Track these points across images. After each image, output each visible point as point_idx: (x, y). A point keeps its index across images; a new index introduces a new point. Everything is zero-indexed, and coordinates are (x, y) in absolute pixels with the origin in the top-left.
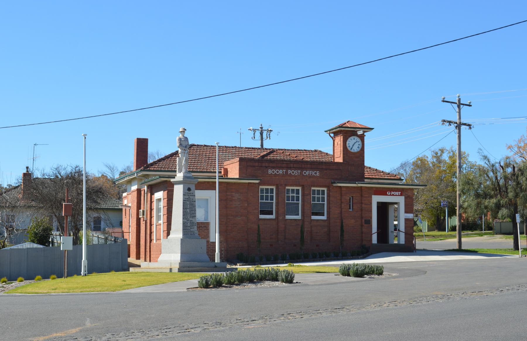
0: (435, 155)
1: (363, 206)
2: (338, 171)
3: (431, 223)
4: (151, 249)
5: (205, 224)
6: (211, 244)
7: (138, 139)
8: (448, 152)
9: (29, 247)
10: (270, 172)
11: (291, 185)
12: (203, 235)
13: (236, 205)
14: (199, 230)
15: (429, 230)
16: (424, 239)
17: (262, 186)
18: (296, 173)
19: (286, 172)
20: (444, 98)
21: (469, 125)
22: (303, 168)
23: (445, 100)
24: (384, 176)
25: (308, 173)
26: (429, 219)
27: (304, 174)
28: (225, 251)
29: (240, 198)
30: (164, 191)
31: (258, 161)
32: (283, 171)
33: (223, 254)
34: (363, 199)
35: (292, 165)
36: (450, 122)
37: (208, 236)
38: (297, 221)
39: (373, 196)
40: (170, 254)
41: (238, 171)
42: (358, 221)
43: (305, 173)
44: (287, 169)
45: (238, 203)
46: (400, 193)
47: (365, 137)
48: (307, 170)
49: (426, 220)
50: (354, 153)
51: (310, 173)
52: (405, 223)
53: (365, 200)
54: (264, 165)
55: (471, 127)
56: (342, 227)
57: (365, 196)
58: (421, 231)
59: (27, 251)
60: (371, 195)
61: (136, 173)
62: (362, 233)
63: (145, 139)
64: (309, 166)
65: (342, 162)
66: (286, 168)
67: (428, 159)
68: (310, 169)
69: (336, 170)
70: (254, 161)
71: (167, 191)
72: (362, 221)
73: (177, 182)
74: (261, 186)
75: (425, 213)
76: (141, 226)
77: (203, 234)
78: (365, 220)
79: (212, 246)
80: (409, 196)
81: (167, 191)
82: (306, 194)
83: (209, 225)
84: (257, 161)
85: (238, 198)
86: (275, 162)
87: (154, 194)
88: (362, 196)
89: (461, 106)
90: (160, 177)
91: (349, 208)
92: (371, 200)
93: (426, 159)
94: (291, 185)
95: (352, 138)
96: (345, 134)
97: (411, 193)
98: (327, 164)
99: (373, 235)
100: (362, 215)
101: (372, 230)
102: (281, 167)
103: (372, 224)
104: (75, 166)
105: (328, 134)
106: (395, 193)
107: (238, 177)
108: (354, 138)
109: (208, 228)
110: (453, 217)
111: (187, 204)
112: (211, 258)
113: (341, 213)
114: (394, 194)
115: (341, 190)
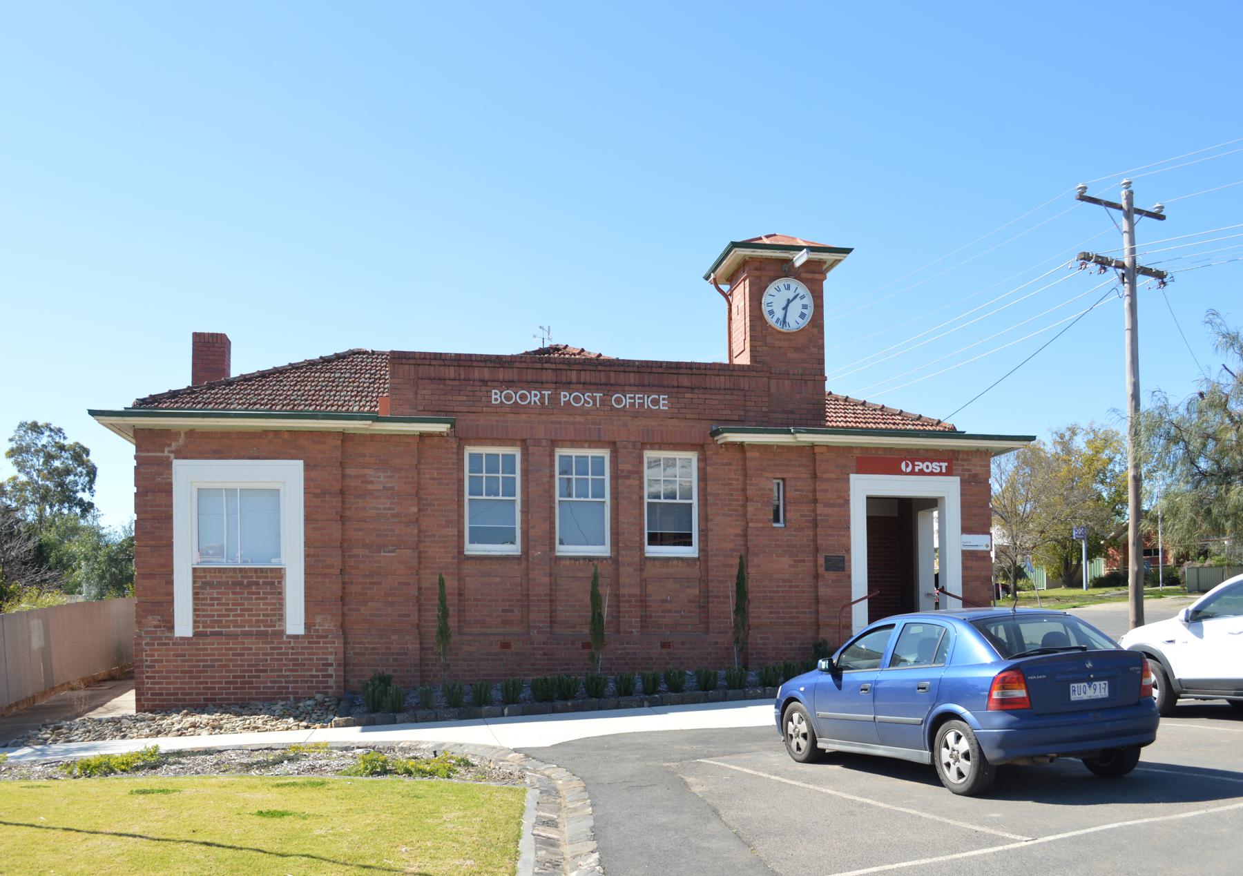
0: (1060, 440)
1: (820, 509)
2: (732, 394)
3: (1054, 573)
6: (290, 642)
8: (1085, 432)
10: (496, 400)
11: (572, 441)
12: (262, 613)
13: (379, 509)
15: (1050, 586)
16: (1039, 605)
17: (474, 445)
18: (589, 403)
19: (554, 399)
20: (1085, 188)
21: (1160, 275)
22: (612, 385)
23: (1088, 194)
24: (904, 424)
25: (628, 401)
26: (1049, 563)
27: (577, 394)
28: (339, 665)
29: (392, 488)
32: (542, 397)
33: (331, 676)
34: (817, 488)
35: (573, 376)
36: (1103, 263)
38: (596, 562)
39: (853, 477)
42: (804, 561)
43: (619, 401)
44: (556, 389)
45: (385, 503)
46: (944, 465)
48: (624, 391)
49: (1044, 567)
50: (788, 333)
51: (637, 401)
52: (965, 568)
53: (826, 491)
55: (1165, 280)
56: (741, 580)
57: (825, 476)
58: (1033, 588)
60: (848, 474)
64: (632, 378)
65: (749, 363)
66: (554, 386)
67: (1045, 447)
68: (636, 388)
69: (725, 389)
70: (442, 363)
72: (816, 561)
74: (470, 445)
75: (1041, 552)
77: (262, 610)
78: (826, 556)
79: (293, 648)
80: (975, 476)
82: (622, 471)
83: (282, 577)
84: (451, 360)
85: (385, 488)
86: (517, 365)
88: (815, 476)
89: (1136, 217)
91: (771, 517)
93: (1042, 447)
94: (574, 443)
95: (780, 283)
96: (758, 273)
97: (980, 466)
98: (695, 371)
99: (854, 606)
100: (815, 541)
102: (537, 382)
103: (850, 570)
106: (927, 467)
108: (789, 286)
109: (281, 588)
110: (1095, 561)
112: (290, 690)
113: (745, 535)
114: (925, 470)
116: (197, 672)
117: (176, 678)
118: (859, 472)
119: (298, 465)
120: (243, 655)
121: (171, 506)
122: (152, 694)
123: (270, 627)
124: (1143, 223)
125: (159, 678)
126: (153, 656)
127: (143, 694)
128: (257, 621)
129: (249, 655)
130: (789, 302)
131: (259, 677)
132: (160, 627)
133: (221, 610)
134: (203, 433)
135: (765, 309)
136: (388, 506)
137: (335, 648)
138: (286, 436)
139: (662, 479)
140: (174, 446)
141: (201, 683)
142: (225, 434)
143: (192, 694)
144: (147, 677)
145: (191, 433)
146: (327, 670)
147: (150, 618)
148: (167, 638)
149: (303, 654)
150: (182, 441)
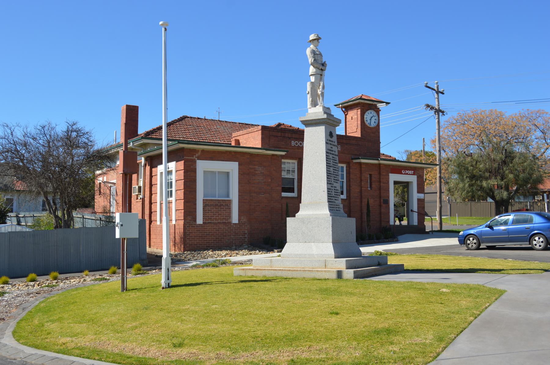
1: (382, 184)
4: (151, 232)
5: (227, 202)
6: (233, 226)
7: (127, 106)
9: (10, 230)
10: (293, 144)
13: (259, 180)
14: (221, 208)
28: (249, 234)
29: (263, 173)
30: (177, 161)
31: (281, 131)
33: (246, 238)
36: (432, 108)
37: (230, 216)
39: (390, 174)
40: (307, 244)
41: (261, 141)
42: (376, 201)
46: (413, 172)
47: (380, 112)
52: (418, 204)
54: (287, 135)
55: (444, 113)
59: (9, 237)
61: (132, 142)
62: (380, 213)
63: (136, 106)
71: (183, 161)
72: (380, 201)
73: (313, 122)
76: (132, 205)
77: (224, 214)
79: (234, 228)
81: (183, 161)
83: (230, 203)
85: (261, 173)
87: (157, 167)
90: (179, 143)
92: (388, 178)
95: (369, 111)
96: (363, 108)
101: (389, 211)
104: (72, 123)
105: (340, 109)
107: (260, 146)
109: (230, 207)
111: (330, 159)
115: (361, 167)
116: (204, 237)
117: (197, 239)
118: (391, 173)
119: (236, 164)
120: (219, 230)
121: (196, 177)
122: (189, 245)
123: (227, 220)
124: (440, 94)
125: (191, 239)
126: (190, 231)
127: (186, 245)
128: (223, 218)
129: (221, 230)
130: (372, 117)
131: (223, 238)
132: (191, 220)
133: (211, 214)
134: (207, 151)
135: (365, 119)
136: (262, 179)
137: (247, 228)
138: (233, 153)
139: (291, 170)
140: (197, 155)
141: (205, 241)
142: (214, 152)
143: (202, 245)
144: (188, 239)
145: (203, 151)
146: (245, 236)
147: (188, 217)
148: (194, 224)
149: (238, 230)
150: (199, 153)
